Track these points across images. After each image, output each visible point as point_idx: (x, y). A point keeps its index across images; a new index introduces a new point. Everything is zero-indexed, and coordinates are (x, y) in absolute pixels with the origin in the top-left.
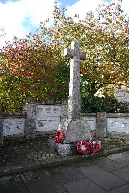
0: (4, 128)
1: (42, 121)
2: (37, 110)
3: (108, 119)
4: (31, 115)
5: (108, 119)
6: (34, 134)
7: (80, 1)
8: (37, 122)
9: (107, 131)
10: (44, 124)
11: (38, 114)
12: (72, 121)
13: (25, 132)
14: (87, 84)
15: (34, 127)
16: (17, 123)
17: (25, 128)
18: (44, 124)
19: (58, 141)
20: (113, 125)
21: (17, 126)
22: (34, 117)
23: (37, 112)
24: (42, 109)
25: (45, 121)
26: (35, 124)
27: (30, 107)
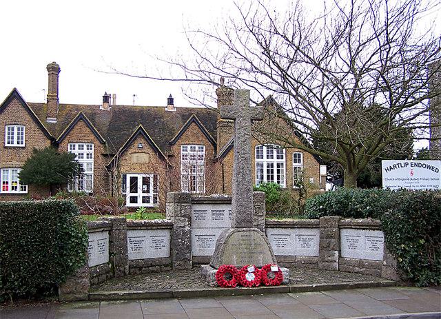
0: (129, 246)
1: (205, 237)
2: (194, 216)
3: (344, 232)
4: (182, 225)
5: (344, 232)
6: (189, 260)
7: (424, 300)
8: (195, 239)
9: (340, 256)
10: (209, 243)
11: (195, 223)
12: (233, 232)
13: (171, 255)
14: (315, 127)
15: (189, 248)
16: (155, 238)
17: (171, 249)
18: (209, 243)
19: (22, 291)
20: (306, 244)
21: (154, 245)
22: (187, 228)
23: (194, 218)
24: (205, 211)
25: (211, 237)
26: (190, 241)
27: (179, 209)
